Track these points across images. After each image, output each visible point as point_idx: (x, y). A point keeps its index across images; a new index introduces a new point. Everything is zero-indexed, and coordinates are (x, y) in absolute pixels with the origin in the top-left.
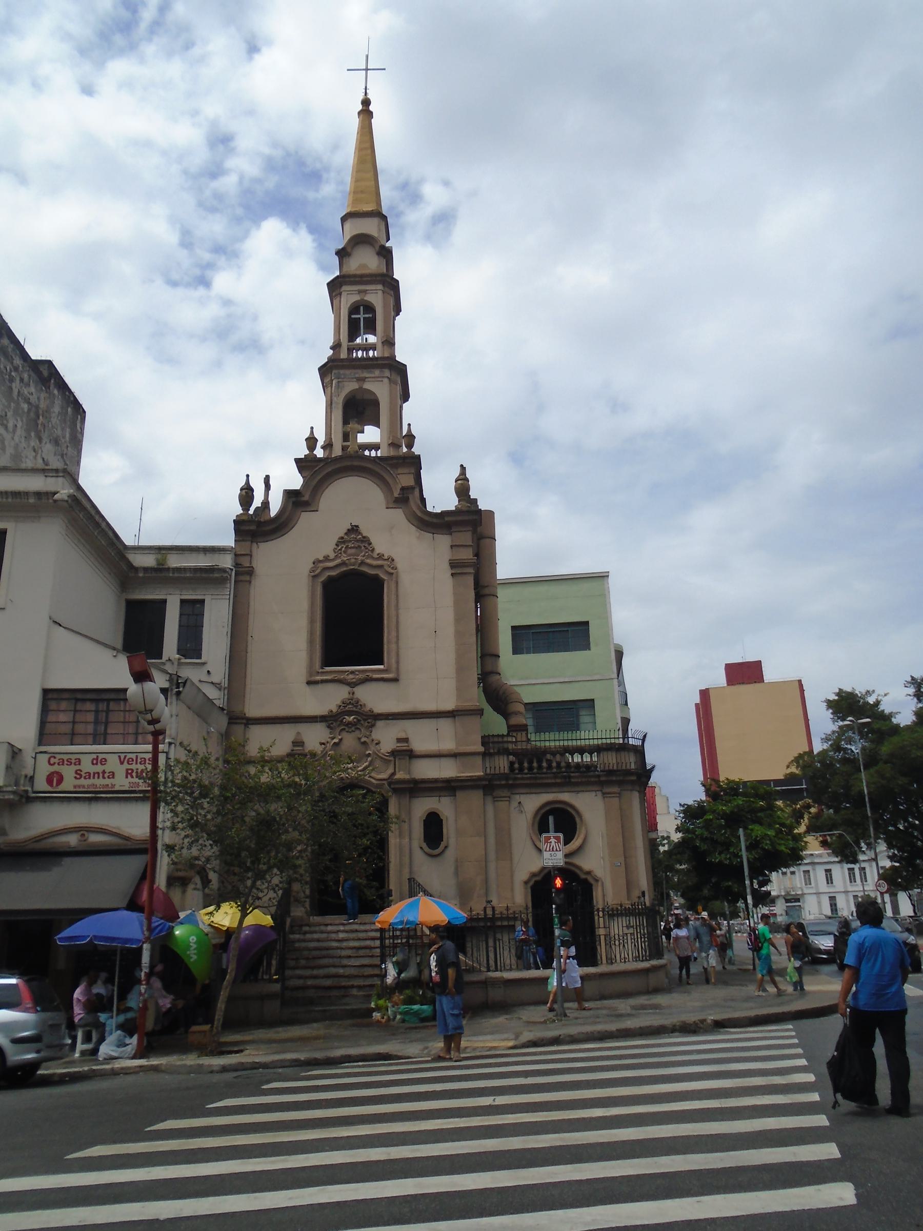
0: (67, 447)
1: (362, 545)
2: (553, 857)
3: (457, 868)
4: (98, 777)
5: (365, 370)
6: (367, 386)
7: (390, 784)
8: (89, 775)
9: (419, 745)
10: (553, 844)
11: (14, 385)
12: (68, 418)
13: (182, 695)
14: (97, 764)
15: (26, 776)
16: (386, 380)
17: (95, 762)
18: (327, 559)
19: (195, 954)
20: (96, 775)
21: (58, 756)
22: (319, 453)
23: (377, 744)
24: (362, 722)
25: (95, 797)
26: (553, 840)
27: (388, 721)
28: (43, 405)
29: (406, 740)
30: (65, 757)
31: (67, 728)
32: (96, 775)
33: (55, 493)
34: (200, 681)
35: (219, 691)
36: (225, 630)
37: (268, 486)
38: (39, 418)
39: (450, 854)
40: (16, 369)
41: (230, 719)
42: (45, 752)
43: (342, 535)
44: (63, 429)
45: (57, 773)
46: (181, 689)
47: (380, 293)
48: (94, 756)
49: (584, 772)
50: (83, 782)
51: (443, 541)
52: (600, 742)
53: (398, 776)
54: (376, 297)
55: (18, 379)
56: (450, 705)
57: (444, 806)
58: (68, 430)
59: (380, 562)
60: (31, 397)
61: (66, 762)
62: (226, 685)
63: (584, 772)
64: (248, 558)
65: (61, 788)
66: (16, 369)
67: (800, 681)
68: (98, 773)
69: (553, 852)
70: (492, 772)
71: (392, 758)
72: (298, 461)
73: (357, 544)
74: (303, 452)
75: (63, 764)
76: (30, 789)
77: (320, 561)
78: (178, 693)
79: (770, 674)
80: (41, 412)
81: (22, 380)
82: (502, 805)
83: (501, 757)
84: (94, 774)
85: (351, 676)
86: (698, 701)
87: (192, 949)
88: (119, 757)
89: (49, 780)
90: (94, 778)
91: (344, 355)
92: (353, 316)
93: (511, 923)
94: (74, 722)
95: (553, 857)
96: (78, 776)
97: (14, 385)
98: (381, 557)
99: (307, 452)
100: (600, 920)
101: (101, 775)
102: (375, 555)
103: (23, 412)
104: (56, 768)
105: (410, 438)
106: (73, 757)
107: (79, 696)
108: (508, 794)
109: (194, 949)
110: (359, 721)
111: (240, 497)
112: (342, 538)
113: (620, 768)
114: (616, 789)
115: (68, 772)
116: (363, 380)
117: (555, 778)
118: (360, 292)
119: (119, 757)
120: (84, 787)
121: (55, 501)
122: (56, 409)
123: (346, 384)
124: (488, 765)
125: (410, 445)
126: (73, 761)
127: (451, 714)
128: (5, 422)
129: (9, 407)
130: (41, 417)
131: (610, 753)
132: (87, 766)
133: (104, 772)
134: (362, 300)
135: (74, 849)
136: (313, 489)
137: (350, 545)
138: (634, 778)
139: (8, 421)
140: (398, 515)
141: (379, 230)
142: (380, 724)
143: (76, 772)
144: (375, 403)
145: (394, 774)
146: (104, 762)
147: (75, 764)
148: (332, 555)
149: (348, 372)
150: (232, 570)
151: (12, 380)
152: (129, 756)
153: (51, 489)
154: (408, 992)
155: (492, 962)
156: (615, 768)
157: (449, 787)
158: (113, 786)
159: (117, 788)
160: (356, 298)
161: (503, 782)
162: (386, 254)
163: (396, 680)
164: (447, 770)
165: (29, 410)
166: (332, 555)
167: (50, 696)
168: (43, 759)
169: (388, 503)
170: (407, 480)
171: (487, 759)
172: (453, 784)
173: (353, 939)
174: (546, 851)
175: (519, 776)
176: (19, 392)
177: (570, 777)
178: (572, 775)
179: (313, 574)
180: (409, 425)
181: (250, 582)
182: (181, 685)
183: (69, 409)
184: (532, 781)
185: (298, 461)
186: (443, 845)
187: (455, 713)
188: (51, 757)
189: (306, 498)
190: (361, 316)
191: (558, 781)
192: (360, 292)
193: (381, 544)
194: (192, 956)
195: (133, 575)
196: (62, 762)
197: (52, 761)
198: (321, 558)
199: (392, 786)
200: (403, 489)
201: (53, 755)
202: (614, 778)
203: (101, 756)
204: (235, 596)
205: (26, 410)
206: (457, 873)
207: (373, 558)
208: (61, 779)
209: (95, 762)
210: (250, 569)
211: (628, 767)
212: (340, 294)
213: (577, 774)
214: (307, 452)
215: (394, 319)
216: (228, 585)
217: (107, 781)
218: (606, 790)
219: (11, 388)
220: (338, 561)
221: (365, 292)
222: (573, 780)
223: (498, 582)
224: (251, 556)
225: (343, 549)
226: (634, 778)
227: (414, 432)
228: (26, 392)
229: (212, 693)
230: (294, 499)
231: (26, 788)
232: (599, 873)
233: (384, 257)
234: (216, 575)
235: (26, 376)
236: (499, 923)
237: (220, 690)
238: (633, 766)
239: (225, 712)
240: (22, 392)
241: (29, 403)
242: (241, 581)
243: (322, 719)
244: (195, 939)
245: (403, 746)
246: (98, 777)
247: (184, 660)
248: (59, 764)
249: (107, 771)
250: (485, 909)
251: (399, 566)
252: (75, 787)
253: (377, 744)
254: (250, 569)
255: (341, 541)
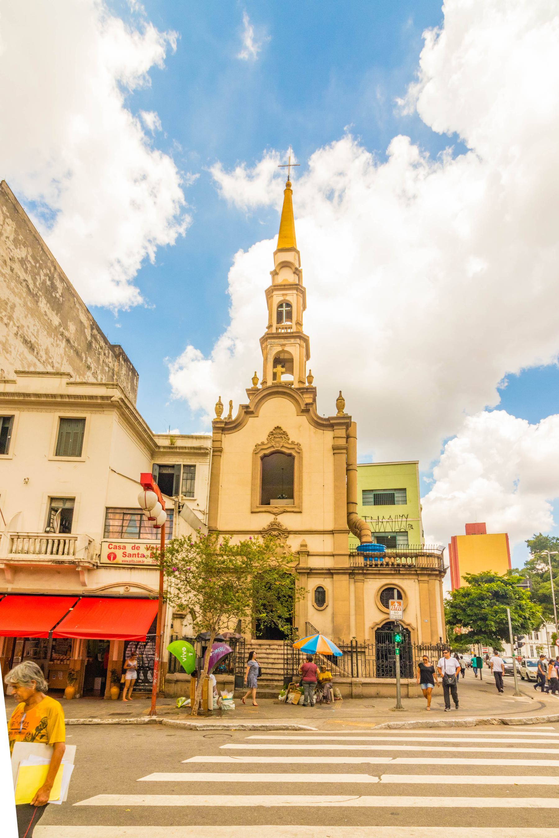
0: (129, 393)
1: (283, 436)
2: (396, 614)
3: (333, 618)
4: (135, 557)
5: (286, 340)
6: (287, 348)
7: (296, 570)
8: (130, 555)
9: (312, 548)
10: (396, 606)
11: (100, 356)
12: (129, 378)
13: (181, 513)
14: (134, 549)
15: (96, 555)
16: (298, 345)
17: (133, 548)
18: (263, 444)
19: (185, 657)
20: (134, 556)
21: (114, 544)
22: (259, 386)
23: (289, 547)
24: (281, 535)
25: (133, 567)
26: (396, 604)
27: (296, 535)
28: (116, 369)
29: (306, 546)
30: (118, 545)
31: (118, 529)
32: (134, 556)
33: (111, 397)
34: (193, 509)
35: (203, 515)
36: (207, 482)
37: (231, 405)
38: (114, 376)
39: (329, 610)
40: (101, 348)
41: (209, 531)
42: (107, 542)
43: (272, 430)
44: (127, 383)
45: (113, 553)
46: (181, 509)
47: (295, 295)
48: (133, 545)
49: (408, 568)
50: (127, 559)
51: (329, 435)
52: (418, 551)
53: (301, 566)
54: (292, 297)
55: (103, 353)
56: (330, 528)
57: (326, 583)
58: (130, 384)
59: (293, 446)
60: (110, 364)
61: (118, 548)
62: (208, 512)
63: (408, 568)
64: (220, 442)
65: (115, 562)
66: (101, 348)
67: (506, 534)
68: (135, 554)
69: (396, 611)
70: (354, 566)
71: (298, 556)
72: (247, 390)
73: (280, 436)
74: (251, 386)
75: (116, 549)
76: (99, 562)
77: (259, 445)
78: (179, 512)
79: (490, 530)
80: (115, 373)
81: (105, 354)
82: (359, 584)
83: (360, 557)
84: (133, 554)
85: (276, 509)
86: (450, 542)
87: (183, 654)
88: (147, 546)
89: (109, 557)
90: (133, 557)
91: (274, 331)
92: (279, 309)
93: (363, 650)
94: (123, 526)
95: (396, 614)
96: (124, 556)
97: (100, 356)
98: (293, 443)
99: (253, 386)
100: (415, 652)
101: (137, 556)
102: (290, 442)
103: (106, 371)
104: (112, 550)
105: (310, 377)
106: (122, 545)
107: (125, 511)
108: (363, 579)
109: (185, 655)
110: (280, 534)
111: (216, 409)
112: (272, 432)
113: (429, 567)
114: (426, 578)
115: (119, 553)
116: (284, 345)
117: (391, 570)
118: (283, 295)
119: (147, 546)
120: (127, 561)
121: (112, 401)
122: (124, 371)
123: (275, 348)
124: (352, 562)
125: (310, 382)
126: (122, 547)
127: (332, 532)
128: (96, 376)
129: (98, 368)
130: (115, 375)
131: (423, 557)
132: (129, 550)
133: (138, 554)
134: (285, 300)
135: (122, 596)
136: (256, 404)
137: (276, 436)
138: (437, 573)
139: (98, 376)
140: (304, 419)
141: (295, 259)
142: (291, 536)
143: (123, 553)
144: (291, 360)
145: (298, 564)
146: (138, 548)
147: (123, 549)
148: (266, 442)
149: (276, 341)
150: (211, 449)
151: (99, 354)
152: (152, 545)
153: (111, 395)
154: (165, 573)
155: (355, 672)
156: (426, 566)
157: (330, 573)
158: (143, 562)
159: (145, 563)
160: (281, 298)
161: (361, 572)
162: (297, 272)
163: (300, 512)
164: (328, 563)
165: (109, 371)
166: (266, 442)
167: (110, 511)
168: (105, 545)
169: (297, 413)
170: (308, 399)
171: (352, 558)
172: (332, 571)
173: (275, 654)
174: (392, 610)
175: (370, 569)
176: (103, 360)
177: (399, 570)
178: (401, 569)
179: (255, 452)
180: (310, 370)
181: (221, 456)
182: (181, 507)
183: (130, 373)
184: (377, 572)
185: (247, 390)
186: (325, 604)
187: (334, 532)
188: (110, 544)
189: (252, 409)
190: (284, 309)
191: (393, 572)
192: (283, 295)
193: (293, 437)
194: (183, 658)
195: (157, 450)
196: (116, 547)
197: (111, 546)
198: (260, 443)
199: (298, 571)
200: (307, 404)
201: (111, 543)
202: (425, 572)
203: (137, 545)
204: (213, 464)
205: (107, 370)
206: (333, 621)
207: (288, 443)
208: (115, 558)
209: (133, 548)
210: (221, 449)
211: (434, 567)
212: (272, 296)
213: (403, 569)
214: (253, 386)
215: (302, 313)
216: (209, 457)
217: (141, 559)
218: (421, 578)
219: (99, 358)
220: (269, 445)
221: (286, 295)
222: (401, 572)
223: (358, 465)
224: (221, 441)
225: (273, 438)
226: (437, 573)
227: (312, 374)
228: (107, 361)
229: (200, 516)
230: (245, 410)
231: (96, 561)
232: (414, 625)
233: (298, 275)
234: (202, 451)
235: (106, 352)
236: (359, 650)
237: (204, 514)
238: (437, 566)
239: (207, 527)
240: (105, 361)
241: (109, 367)
242: (216, 455)
243: (260, 532)
244: (185, 649)
245: (303, 549)
246: (135, 557)
247: (184, 498)
248: (114, 548)
249: (140, 553)
250: (351, 641)
251: (304, 450)
252: (123, 561)
253: (289, 547)
254: (221, 449)
255: (272, 434)
